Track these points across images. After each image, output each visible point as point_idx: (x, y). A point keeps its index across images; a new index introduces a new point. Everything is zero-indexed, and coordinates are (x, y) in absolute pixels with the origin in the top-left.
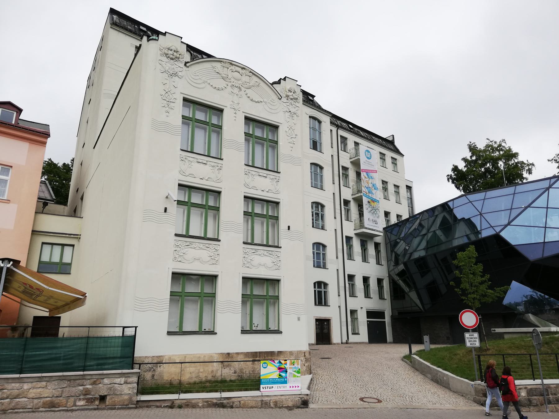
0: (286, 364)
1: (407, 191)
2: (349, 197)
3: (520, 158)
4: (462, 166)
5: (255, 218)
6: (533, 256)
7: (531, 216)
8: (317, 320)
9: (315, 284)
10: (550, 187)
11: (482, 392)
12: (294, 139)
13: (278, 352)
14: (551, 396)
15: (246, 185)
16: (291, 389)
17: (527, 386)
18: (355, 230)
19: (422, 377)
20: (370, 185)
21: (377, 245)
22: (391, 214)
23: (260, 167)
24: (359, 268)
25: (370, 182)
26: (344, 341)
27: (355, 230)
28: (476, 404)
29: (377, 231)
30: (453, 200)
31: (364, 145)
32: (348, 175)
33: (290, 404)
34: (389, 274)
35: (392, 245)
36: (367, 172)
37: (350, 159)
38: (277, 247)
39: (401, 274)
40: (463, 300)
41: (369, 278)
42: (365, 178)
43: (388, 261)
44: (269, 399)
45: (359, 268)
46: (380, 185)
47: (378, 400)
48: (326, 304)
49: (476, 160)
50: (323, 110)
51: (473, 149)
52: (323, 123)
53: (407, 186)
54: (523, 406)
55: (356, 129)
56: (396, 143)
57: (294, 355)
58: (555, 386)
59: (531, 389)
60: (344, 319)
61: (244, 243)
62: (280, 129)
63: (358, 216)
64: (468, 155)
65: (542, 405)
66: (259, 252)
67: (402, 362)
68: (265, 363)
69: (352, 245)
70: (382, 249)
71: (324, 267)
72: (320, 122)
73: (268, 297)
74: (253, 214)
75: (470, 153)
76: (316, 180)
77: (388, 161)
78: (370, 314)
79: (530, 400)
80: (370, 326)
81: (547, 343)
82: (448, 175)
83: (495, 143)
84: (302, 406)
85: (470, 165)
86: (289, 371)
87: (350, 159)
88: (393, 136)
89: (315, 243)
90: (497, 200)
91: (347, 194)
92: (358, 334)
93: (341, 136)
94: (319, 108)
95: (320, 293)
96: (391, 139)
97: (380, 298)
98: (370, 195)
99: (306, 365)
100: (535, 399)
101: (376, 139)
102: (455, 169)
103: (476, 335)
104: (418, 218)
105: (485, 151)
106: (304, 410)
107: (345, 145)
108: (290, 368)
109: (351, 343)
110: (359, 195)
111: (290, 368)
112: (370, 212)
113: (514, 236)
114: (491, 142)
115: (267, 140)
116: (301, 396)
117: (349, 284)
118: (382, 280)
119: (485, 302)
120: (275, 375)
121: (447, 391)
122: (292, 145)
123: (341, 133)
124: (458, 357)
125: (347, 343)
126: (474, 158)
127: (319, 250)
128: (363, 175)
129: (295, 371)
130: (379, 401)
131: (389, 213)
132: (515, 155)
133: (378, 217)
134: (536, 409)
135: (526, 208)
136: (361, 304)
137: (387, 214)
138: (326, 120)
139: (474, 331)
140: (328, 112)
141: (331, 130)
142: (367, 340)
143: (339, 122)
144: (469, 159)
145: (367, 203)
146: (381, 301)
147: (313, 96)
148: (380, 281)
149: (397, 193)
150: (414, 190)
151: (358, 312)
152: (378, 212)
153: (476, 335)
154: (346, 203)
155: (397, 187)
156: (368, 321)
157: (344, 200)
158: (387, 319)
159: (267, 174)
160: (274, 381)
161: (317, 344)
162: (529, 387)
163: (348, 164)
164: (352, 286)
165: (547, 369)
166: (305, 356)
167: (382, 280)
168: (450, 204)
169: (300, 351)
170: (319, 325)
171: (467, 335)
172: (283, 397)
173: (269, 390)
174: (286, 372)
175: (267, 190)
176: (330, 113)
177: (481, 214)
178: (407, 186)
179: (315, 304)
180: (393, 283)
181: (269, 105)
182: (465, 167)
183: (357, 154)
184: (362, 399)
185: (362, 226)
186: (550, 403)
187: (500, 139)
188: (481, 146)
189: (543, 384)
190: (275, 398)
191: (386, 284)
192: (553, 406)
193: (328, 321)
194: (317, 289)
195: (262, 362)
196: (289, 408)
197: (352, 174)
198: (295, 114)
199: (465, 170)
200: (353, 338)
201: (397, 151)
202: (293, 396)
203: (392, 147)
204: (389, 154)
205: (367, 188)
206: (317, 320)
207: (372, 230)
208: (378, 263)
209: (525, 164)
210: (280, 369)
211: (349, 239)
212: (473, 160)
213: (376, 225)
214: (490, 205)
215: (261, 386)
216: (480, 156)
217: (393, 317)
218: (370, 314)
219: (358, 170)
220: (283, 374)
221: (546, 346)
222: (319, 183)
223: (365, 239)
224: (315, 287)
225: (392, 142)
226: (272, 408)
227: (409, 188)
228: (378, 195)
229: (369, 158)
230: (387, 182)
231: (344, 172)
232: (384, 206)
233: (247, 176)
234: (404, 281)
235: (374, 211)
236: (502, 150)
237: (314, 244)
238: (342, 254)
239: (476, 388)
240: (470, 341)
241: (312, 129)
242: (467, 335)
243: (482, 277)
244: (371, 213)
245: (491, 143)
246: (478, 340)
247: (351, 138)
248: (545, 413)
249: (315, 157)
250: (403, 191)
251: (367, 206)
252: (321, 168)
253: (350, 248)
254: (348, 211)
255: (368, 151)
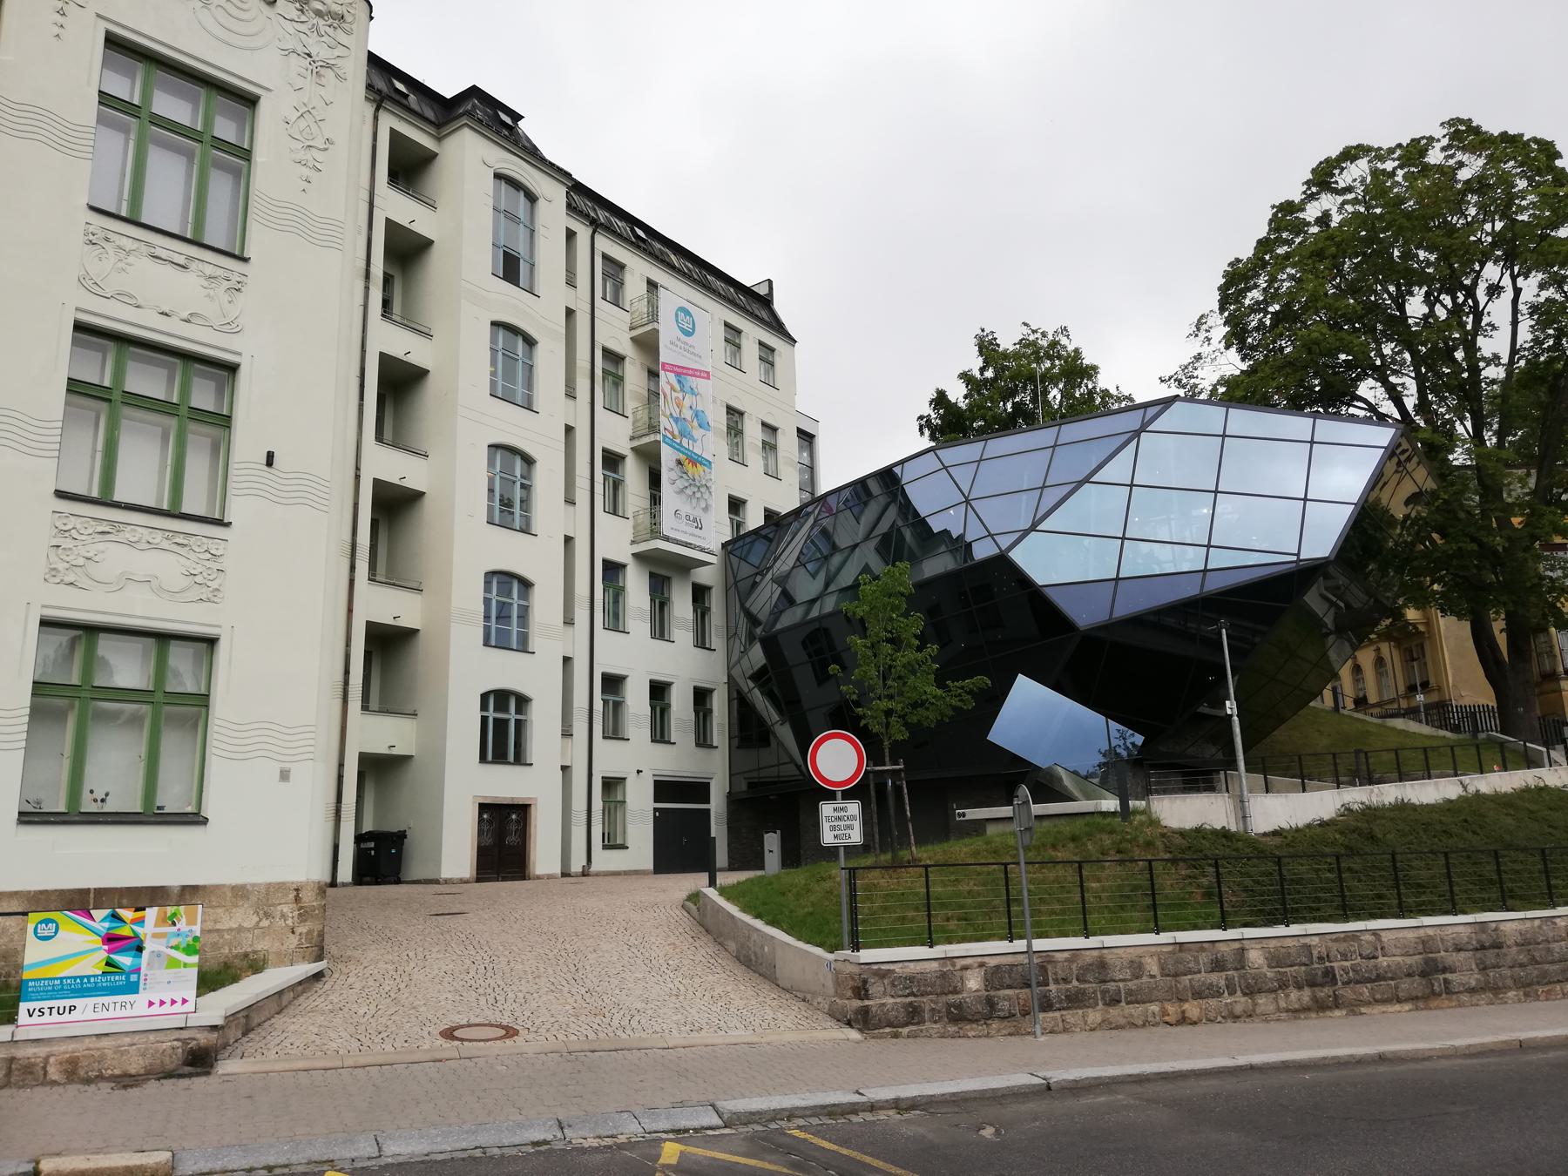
0: (141, 921)
1: (801, 448)
2: (622, 446)
3: (1104, 381)
4: (957, 393)
5: (126, 411)
6: (1085, 615)
7: (1094, 507)
8: (483, 807)
9: (485, 697)
10: (1143, 428)
11: (851, 983)
12: (319, 156)
13: (184, 888)
14: (1052, 987)
15: (87, 283)
16: (156, 1009)
17: (986, 959)
18: (633, 542)
19: (712, 948)
20: (687, 414)
21: (700, 594)
22: (749, 506)
23: (176, 231)
24: (636, 654)
25: (687, 402)
26: (577, 864)
27: (633, 542)
28: (830, 1023)
29: (702, 550)
30: (902, 462)
31: (676, 293)
32: (622, 379)
33: (135, 1065)
34: (729, 676)
35: (740, 589)
36: (678, 374)
37: (632, 329)
38: (220, 523)
39: (759, 677)
40: (860, 718)
41: (669, 684)
42: (672, 388)
43: (731, 636)
44: (42, 1051)
45: (636, 654)
46: (719, 419)
47: (503, 1027)
48: (520, 760)
49: (995, 379)
50: (543, 160)
51: (987, 347)
52: (541, 203)
53: (800, 431)
54: (971, 1021)
55: (658, 246)
56: (778, 306)
57: (254, 899)
58: (1066, 955)
59: (998, 967)
60: (579, 803)
61: (61, 495)
62: (264, 107)
63: (647, 503)
64: (974, 363)
65: (1025, 1013)
66: (127, 535)
67: (679, 913)
68: (47, 921)
69: (623, 589)
70: (716, 602)
71: (523, 647)
72: (532, 198)
73: (159, 697)
74: (116, 396)
75: (981, 359)
76: (509, 375)
77: (750, 352)
78: (664, 789)
79: (990, 1003)
80: (663, 823)
81: (1074, 839)
82: (921, 418)
83: (1044, 335)
84: (187, 1069)
85: (979, 394)
86: (149, 946)
87: (632, 329)
88: (770, 282)
89: (494, 573)
90: (1012, 460)
91: (616, 434)
92: (623, 847)
93: (605, 257)
94: (532, 154)
95: (501, 725)
96: (763, 291)
97: (698, 745)
98: (685, 442)
99: (303, 929)
100: (1007, 997)
101: (718, 284)
102: (940, 400)
103: (854, 808)
104: (808, 514)
105: (1016, 356)
106: (199, 1082)
107: (619, 285)
108: (155, 936)
109: (597, 874)
110: (652, 438)
111: (155, 936)
112: (681, 491)
113: (1047, 562)
114: (1034, 332)
115: (207, 138)
116: (185, 1035)
117: (605, 702)
118: (711, 691)
119: (919, 723)
120: (92, 962)
121: (765, 986)
122: (306, 172)
123: (605, 244)
124: (827, 885)
125: (584, 874)
126: (989, 374)
127: (509, 595)
128: (667, 379)
129: (176, 948)
130: (510, 1032)
131: (744, 502)
132: (1090, 372)
133: (706, 509)
134: (1007, 1026)
135: (1080, 484)
136: (639, 761)
137: (736, 505)
138: (553, 196)
139: (848, 795)
140: (560, 170)
141: (571, 235)
142: (649, 864)
143: (602, 215)
144: (978, 375)
145: (673, 464)
146: (702, 752)
147: (517, 117)
148: (701, 696)
149: (769, 447)
150: (821, 444)
151: (629, 783)
152: (706, 496)
153: (854, 808)
154: (612, 461)
155: (770, 429)
156: (655, 810)
157: (604, 450)
158: (717, 804)
159: (189, 258)
160: (81, 988)
161: (478, 880)
162: (992, 962)
163: (623, 346)
164: (615, 709)
165: (1057, 907)
166: (297, 899)
167: (711, 691)
168: (897, 470)
169: (281, 887)
170: (490, 822)
171: (826, 809)
172: (105, 1043)
173: (55, 1017)
174: (140, 949)
175: (185, 315)
176: (568, 175)
177: (967, 501)
178: (800, 431)
179: (483, 758)
180: (740, 703)
181: (220, 14)
182: (966, 397)
183: (654, 316)
184: (449, 1034)
185: (655, 531)
186: (1046, 1005)
187: (1057, 326)
188: (1007, 342)
189: (1029, 952)
190: (71, 1046)
191: (719, 705)
192: (1057, 1014)
193: (523, 809)
194: (492, 714)
195: (34, 918)
196: (127, 1081)
197: (633, 374)
198: (329, 66)
199: (963, 404)
200: (604, 860)
201: (777, 326)
202: (152, 1037)
203: (764, 314)
204: (753, 333)
205: (676, 420)
206: (483, 807)
207: (687, 545)
208: (701, 642)
209: (1111, 396)
210: (111, 940)
211: (613, 569)
212: (986, 380)
213: (700, 531)
214: (994, 476)
215: (23, 1007)
216: (1004, 368)
217: (733, 800)
218: (664, 789)
219: (653, 367)
220: (125, 960)
221: (1071, 845)
222: (520, 390)
223: (664, 570)
224: (484, 707)
225: (766, 301)
226: (54, 1083)
227: (806, 438)
228: (712, 444)
229: (688, 334)
230: (741, 414)
231: (611, 369)
232: (726, 478)
233: (96, 251)
234: (770, 695)
235: (697, 490)
236: (1059, 357)
237: (490, 575)
238: (587, 612)
239: (837, 972)
240: (833, 828)
241: (504, 214)
242: (826, 809)
243: (919, 649)
244: (683, 497)
245: (1032, 338)
246: (857, 825)
247: (638, 269)
248: (1030, 1038)
249: (509, 303)
250: (788, 443)
251: (674, 475)
252: (530, 342)
253: (616, 602)
254: (617, 485)
255: (687, 312)
